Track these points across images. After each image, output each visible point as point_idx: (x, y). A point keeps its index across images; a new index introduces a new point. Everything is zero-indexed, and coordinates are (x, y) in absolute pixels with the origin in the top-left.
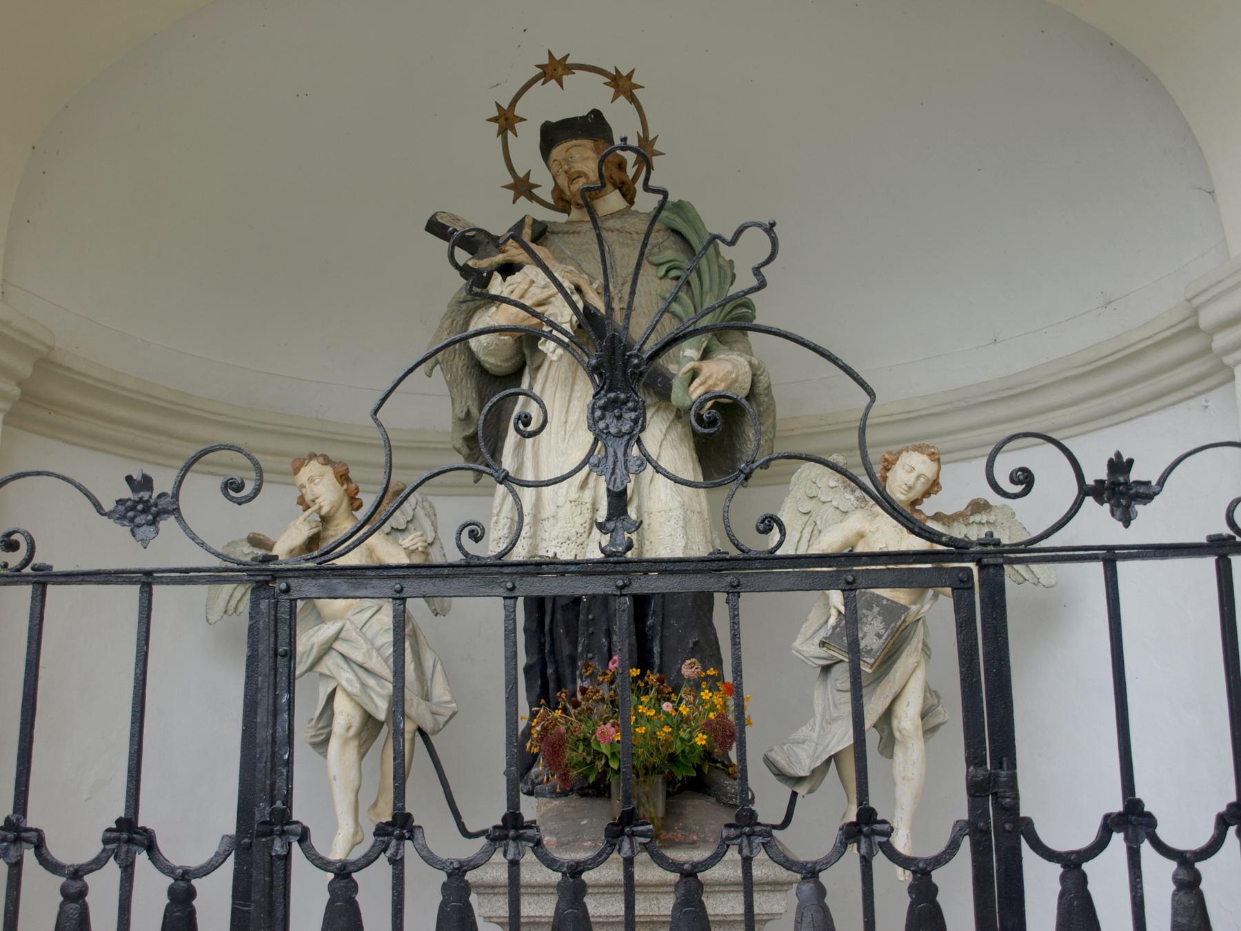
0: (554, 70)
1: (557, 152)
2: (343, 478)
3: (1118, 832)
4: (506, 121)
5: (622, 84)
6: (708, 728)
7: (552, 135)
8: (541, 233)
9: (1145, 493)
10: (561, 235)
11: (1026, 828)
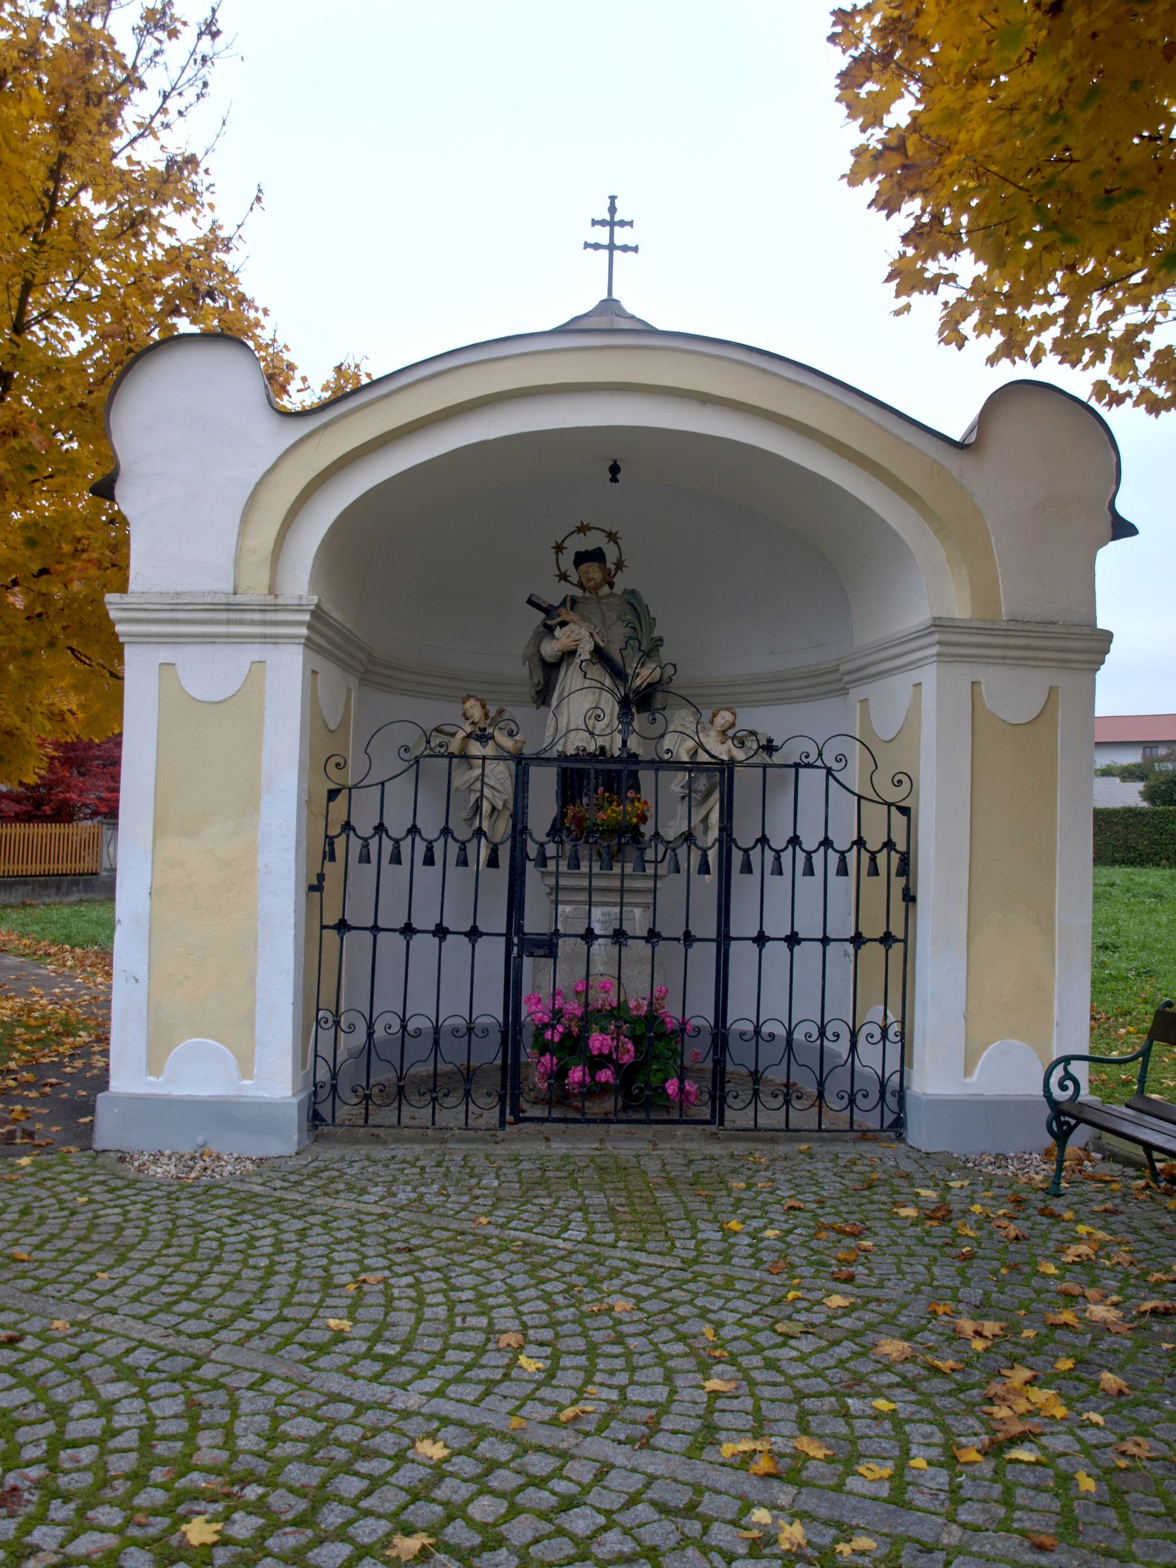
0: (583, 529)
1: (582, 567)
2: (483, 707)
3: (1002, 333)
4: (559, 548)
5: (612, 537)
6: (638, 816)
7: (581, 558)
8: (574, 602)
9: (776, 749)
10: (732, 1491)
11: (734, 841)
